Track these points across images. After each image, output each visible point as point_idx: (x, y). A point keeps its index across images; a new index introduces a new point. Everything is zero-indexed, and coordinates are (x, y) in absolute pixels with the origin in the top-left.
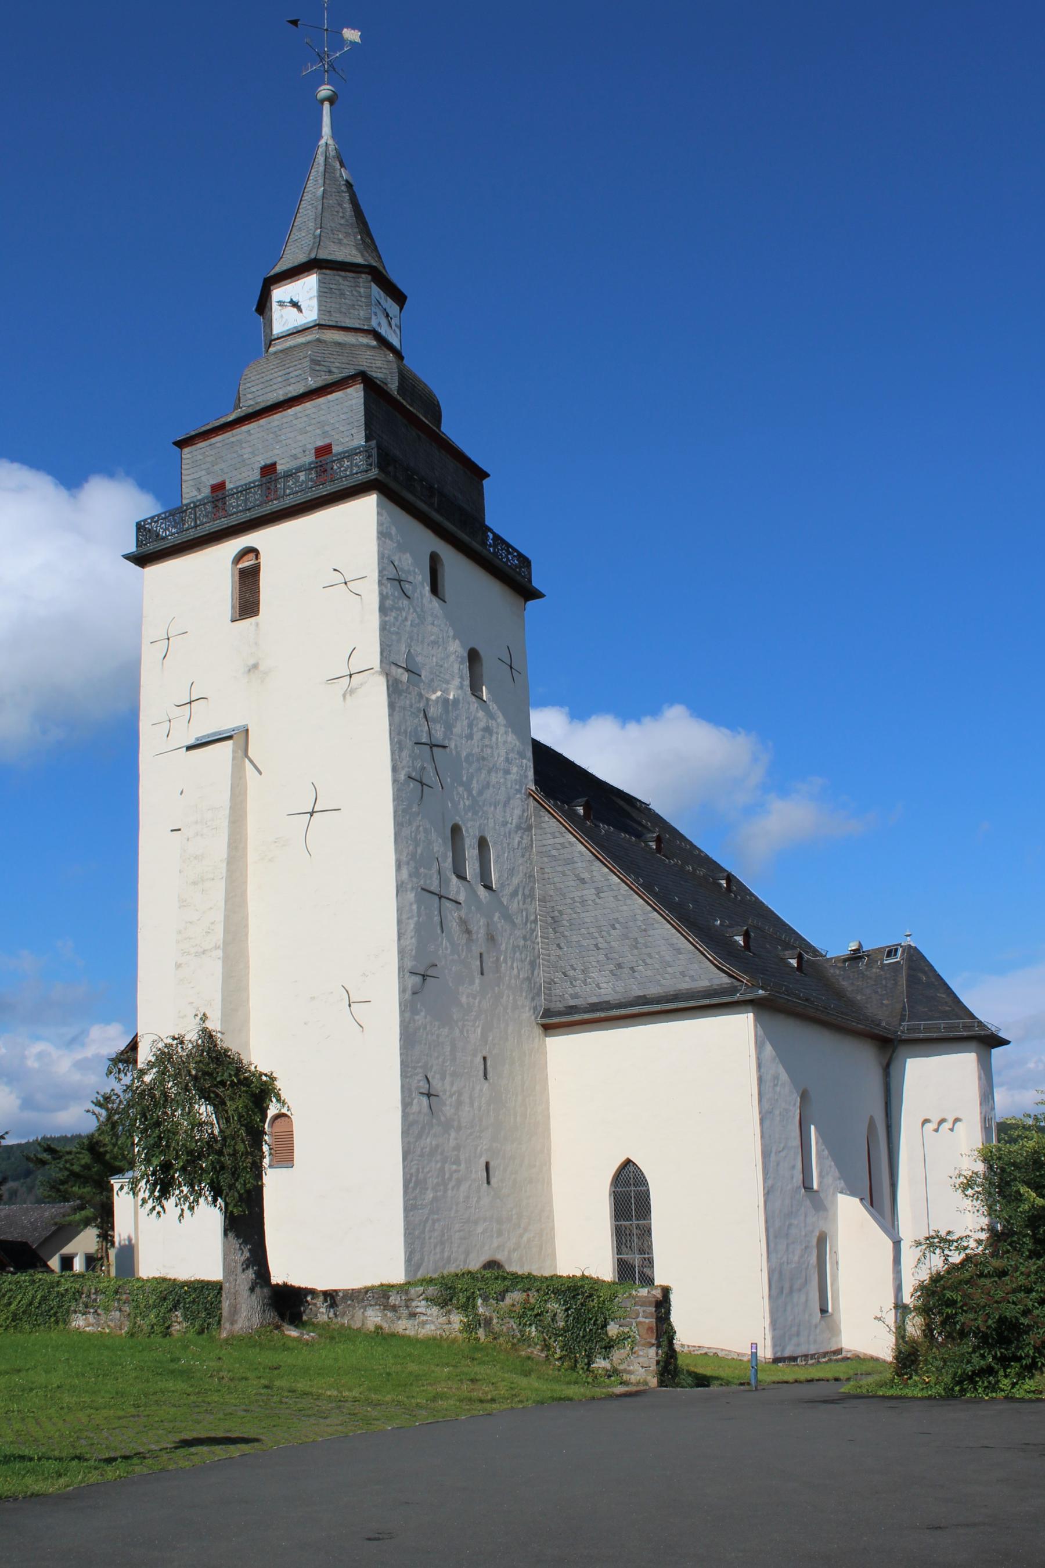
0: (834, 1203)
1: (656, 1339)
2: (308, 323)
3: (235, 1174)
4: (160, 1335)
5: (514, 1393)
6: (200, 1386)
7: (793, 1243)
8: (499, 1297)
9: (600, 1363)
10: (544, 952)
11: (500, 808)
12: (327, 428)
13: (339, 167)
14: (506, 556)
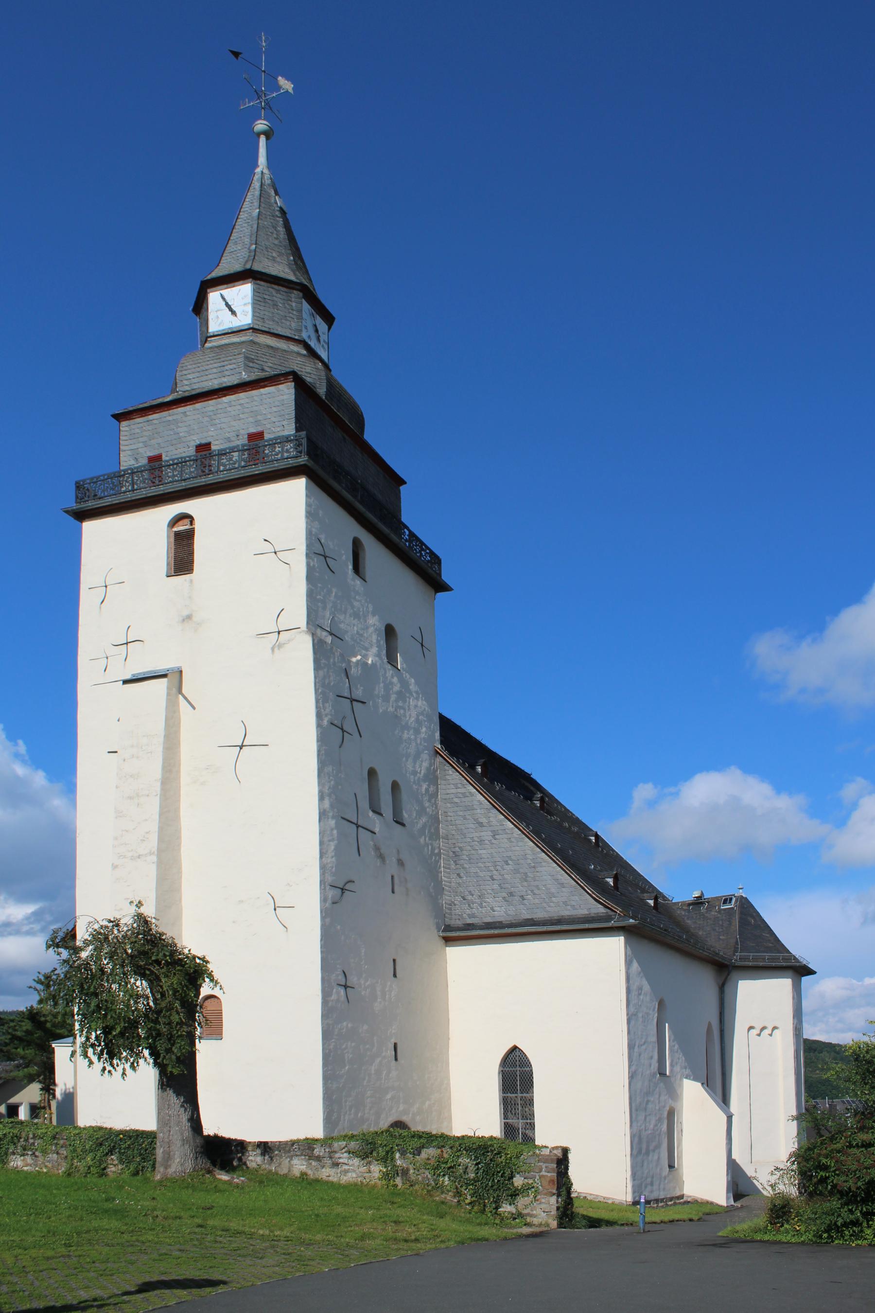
0: (681, 1086)
1: (557, 1190)
2: (243, 326)
3: (171, 1039)
4: (96, 1175)
5: (436, 1234)
6: (135, 1224)
7: (650, 1115)
8: (416, 1152)
9: (506, 1208)
10: (446, 879)
11: (410, 760)
12: (259, 418)
13: (274, 195)
14: (420, 552)
